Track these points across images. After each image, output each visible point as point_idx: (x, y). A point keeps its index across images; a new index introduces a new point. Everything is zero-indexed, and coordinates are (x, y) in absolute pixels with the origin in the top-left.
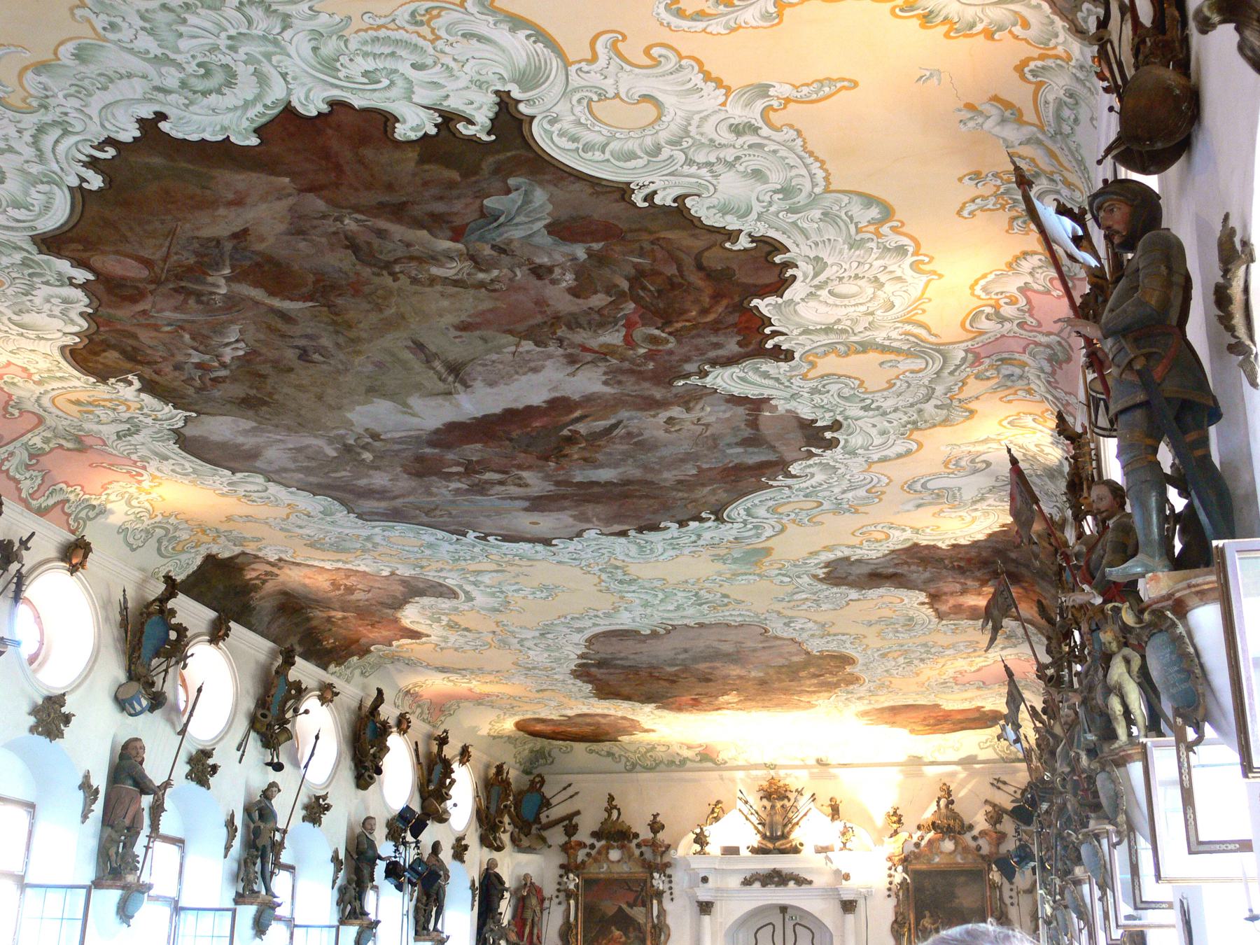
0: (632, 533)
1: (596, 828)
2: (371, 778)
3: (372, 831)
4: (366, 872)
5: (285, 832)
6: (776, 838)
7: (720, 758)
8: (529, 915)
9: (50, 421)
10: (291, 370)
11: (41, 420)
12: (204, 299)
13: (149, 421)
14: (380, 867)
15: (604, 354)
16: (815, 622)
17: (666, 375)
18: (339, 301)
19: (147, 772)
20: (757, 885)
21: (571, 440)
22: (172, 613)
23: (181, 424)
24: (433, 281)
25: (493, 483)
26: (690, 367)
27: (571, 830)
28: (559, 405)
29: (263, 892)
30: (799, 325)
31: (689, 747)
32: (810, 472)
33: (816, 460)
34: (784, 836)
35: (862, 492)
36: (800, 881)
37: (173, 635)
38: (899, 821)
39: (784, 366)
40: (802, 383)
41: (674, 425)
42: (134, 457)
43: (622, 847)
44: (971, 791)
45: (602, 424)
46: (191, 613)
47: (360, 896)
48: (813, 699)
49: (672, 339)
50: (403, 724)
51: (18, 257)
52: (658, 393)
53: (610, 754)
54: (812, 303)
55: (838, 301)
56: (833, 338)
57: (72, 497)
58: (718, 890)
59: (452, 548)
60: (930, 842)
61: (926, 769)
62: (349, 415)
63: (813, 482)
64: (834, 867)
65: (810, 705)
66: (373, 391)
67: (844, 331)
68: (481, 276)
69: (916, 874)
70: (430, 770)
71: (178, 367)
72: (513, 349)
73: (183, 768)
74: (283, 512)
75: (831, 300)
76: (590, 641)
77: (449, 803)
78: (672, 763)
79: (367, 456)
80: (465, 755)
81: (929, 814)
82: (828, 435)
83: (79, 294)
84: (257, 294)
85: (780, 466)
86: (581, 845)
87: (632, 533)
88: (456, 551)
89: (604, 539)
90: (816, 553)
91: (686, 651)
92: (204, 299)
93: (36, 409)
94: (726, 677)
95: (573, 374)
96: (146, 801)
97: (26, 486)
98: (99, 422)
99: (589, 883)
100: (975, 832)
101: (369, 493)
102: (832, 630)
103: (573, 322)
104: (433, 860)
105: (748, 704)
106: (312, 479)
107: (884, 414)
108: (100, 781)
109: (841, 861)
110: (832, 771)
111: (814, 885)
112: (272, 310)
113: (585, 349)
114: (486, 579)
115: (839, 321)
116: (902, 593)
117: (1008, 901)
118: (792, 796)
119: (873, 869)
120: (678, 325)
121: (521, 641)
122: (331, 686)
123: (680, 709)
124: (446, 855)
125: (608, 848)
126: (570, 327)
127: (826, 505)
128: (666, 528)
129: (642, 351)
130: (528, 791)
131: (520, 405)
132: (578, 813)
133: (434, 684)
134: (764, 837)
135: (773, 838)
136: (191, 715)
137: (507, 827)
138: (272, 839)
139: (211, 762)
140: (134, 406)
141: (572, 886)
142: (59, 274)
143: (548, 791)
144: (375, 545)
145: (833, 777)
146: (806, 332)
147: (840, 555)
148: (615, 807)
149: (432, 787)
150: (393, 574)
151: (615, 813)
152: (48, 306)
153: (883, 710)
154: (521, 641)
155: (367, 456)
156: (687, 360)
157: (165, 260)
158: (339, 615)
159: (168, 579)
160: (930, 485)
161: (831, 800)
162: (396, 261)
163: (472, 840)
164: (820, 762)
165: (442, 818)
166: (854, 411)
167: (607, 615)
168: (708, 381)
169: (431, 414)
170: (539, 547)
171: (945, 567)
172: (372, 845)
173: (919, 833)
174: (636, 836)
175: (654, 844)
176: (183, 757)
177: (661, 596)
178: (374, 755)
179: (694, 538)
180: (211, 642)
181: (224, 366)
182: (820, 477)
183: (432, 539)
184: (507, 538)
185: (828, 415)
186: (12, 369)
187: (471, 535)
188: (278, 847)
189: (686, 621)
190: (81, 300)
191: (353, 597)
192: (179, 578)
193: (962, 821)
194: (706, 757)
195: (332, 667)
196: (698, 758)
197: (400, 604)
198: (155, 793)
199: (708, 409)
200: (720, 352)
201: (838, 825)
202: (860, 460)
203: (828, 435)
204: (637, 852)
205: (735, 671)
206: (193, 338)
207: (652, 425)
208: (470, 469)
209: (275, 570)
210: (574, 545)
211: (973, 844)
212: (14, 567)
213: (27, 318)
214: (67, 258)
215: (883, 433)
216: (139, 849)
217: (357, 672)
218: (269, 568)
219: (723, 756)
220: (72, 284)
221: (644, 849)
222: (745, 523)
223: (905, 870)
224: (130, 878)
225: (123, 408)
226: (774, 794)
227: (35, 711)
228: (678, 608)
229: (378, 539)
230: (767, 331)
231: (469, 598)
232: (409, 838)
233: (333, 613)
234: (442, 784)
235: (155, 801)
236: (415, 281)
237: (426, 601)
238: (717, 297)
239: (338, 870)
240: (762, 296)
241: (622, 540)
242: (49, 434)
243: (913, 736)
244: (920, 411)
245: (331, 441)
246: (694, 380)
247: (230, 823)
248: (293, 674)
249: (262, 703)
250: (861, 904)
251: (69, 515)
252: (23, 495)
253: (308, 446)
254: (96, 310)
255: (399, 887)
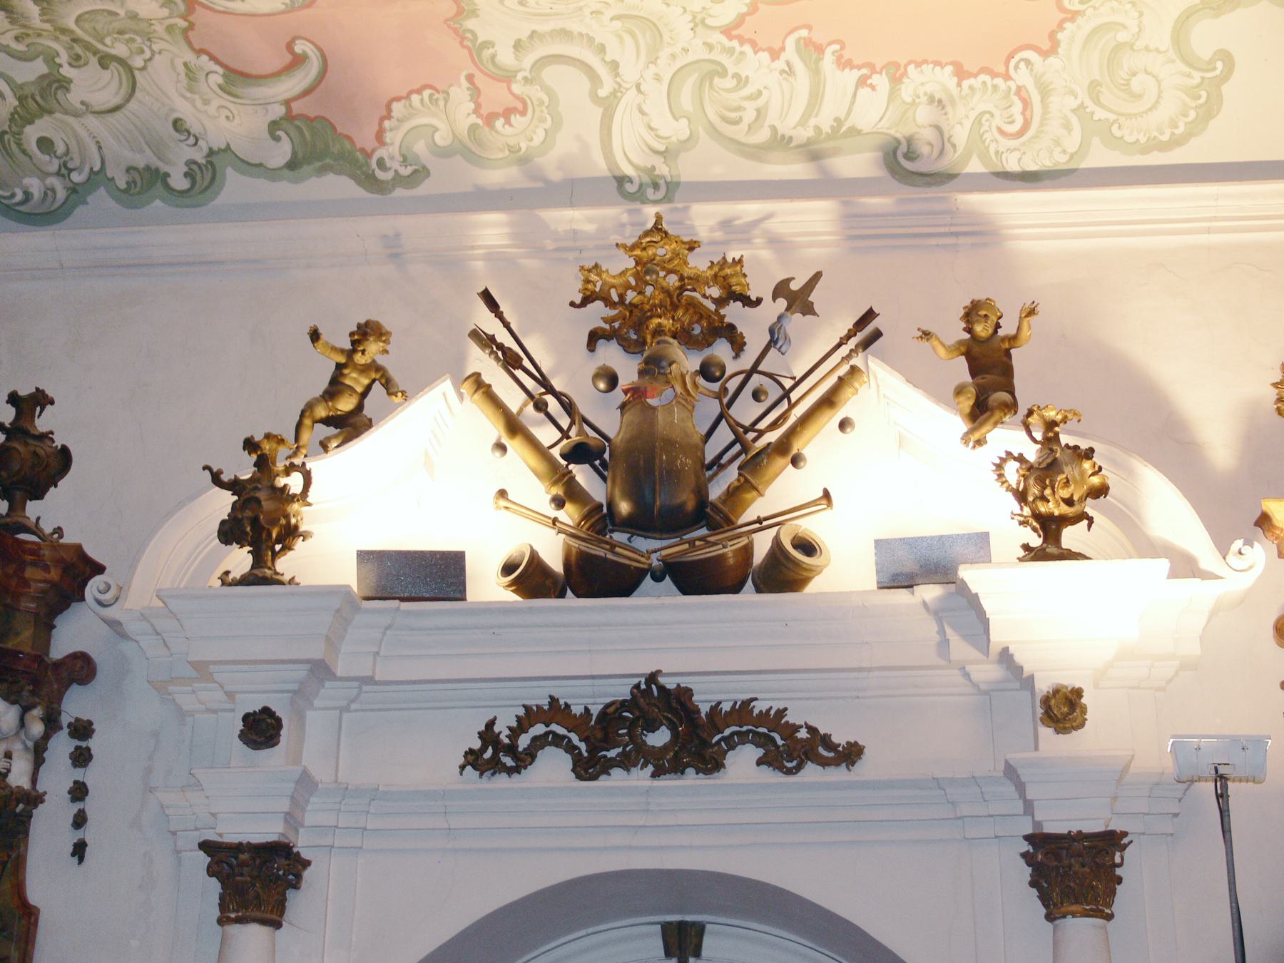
6: (663, 506)
7: (390, 151)
20: (553, 767)
34: (716, 517)
36: (794, 749)
78: (146, 182)
118: (753, 325)
161: (972, 313)
176: (1038, 703)
196: (282, 152)
201: (1009, 438)
226: (669, 312)
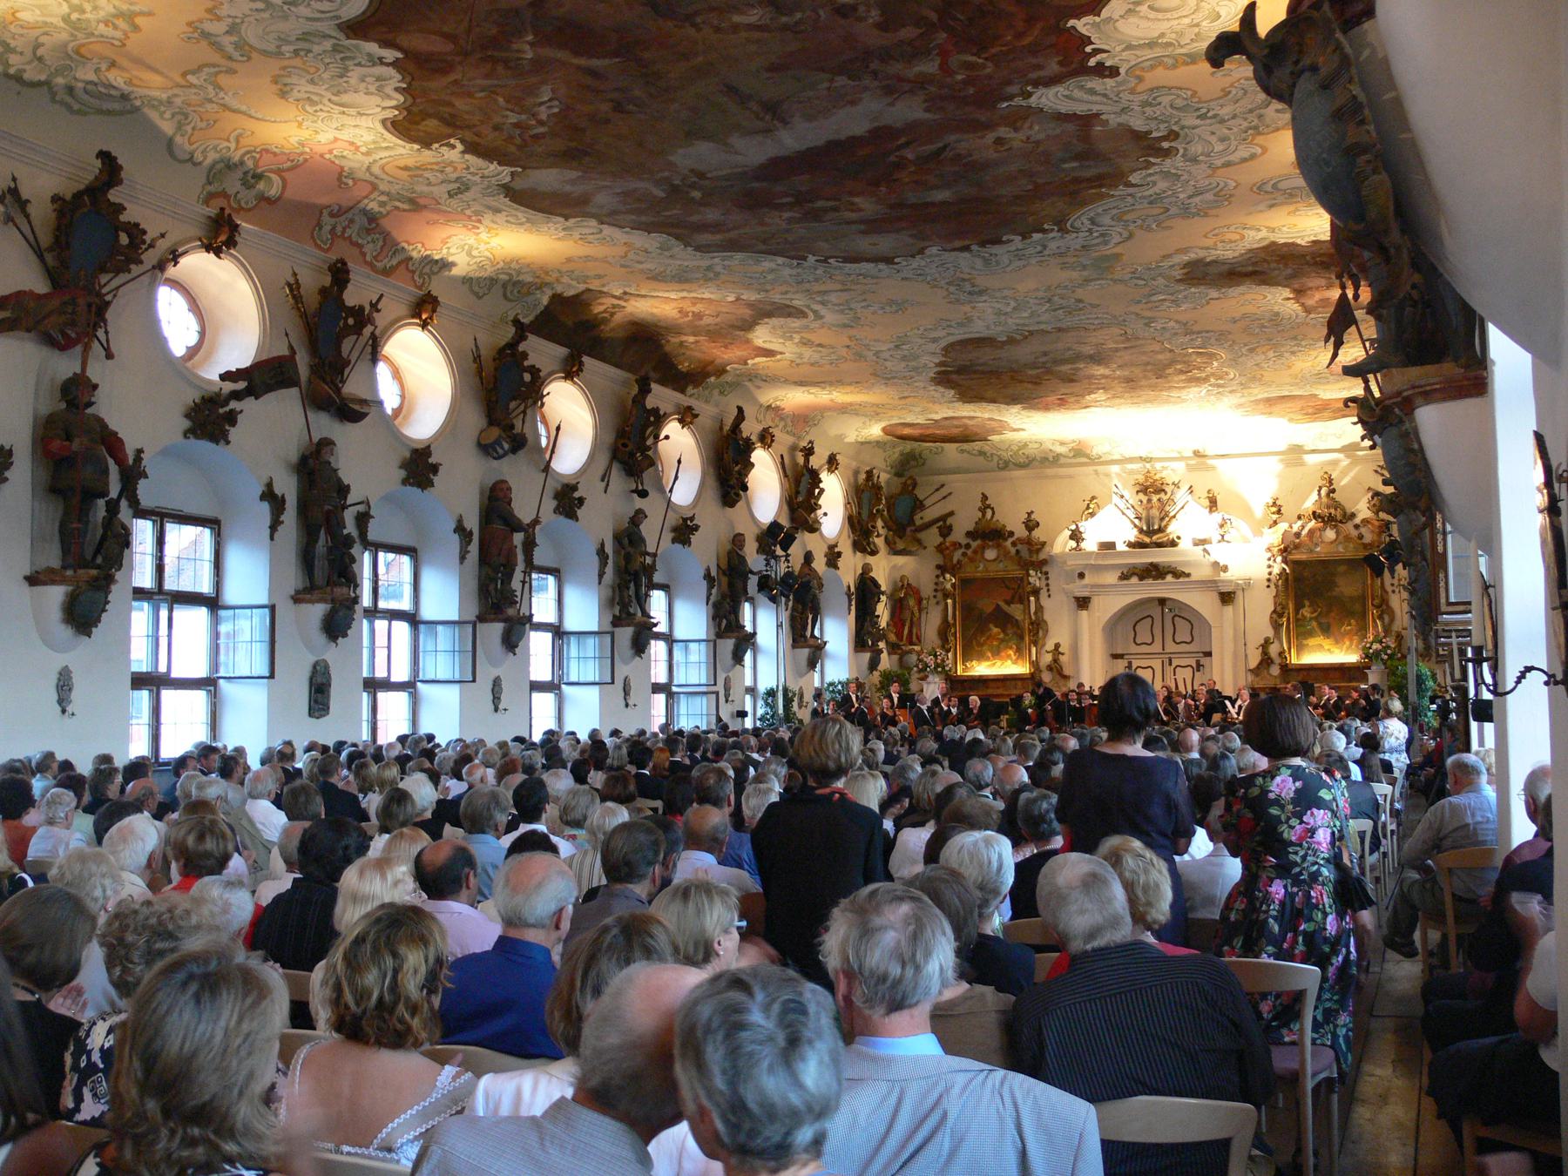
0: (974, 247)
1: (971, 527)
2: (738, 495)
3: (742, 547)
4: (739, 585)
5: (655, 555)
8: (907, 615)
9: (382, 187)
10: (608, 121)
11: (374, 187)
12: (512, 64)
13: (477, 178)
14: (753, 582)
15: (921, 82)
16: (1177, 322)
17: (988, 97)
18: (646, 55)
19: (516, 512)
20: (1134, 580)
21: (900, 165)
22: (525, 355)
23: (508, 179)
24: (736, 28)
25: (825, 210)
26: (1014, 89)
27: (946, 531)
28: (881, 135)
29: (639, 614)
30: (1120, 42)
31: (1062, 444)
32: (1151, 180)
33: (1157, 169)
35: (1209, 196)
36: (1178, 574)
37: (527, 377)
38: (1279, 512)
39: (1110, 82)
40: (1131, 97)
41: (1002, 145)
42: (468, 212)
43: (998, 546)
44: (1354, 478)
45: (930, 148)
46: (541, 352)
47: (735, 611)
48: (1183, 394)
49: (989, 64)
50: (766, 438)
51: (328, 45)
52: (983, 117)
53: (982, 453)
54: (1132, 20)
55: (1160, 16)
56: (1158, 52)
57: (414, 254)
58: (1093, 586)
59: (794, 272)
60: (1311, 532)
61: (1311, 459)
62: (671, 158)
63: (1156, 189)
64: (1212, 559)
65: (1181, 400)
66: (694, 134)
67: (1169, 44)
68: (784, 19)
69: (1296, 565)
70: (797, 482)
71: (496, 128)
72: (826, 85)
73: (550, 504)
74: (621, 250)
75: (1153, 15)
76: (947, 350)
77: (820, 512)
78: (1045, 459)
79: (696, 194)
80: (832, 463)
81: (1310, 503)
82: (1165, 145)
83: (391, 71)
84: (560, 55)
85: (1117, 178)
86: (957, 545)
87: (974, 247)
88: (798, 275)
89: (947, 254)
90: (1169, 256)
91: (1045, 354)
92: (512, 64)
93: (367, 177)
94: (1090, 377)
95: (892, 104)
96: (518, 538)
97: (370, 250)
98: (429, 184)
99: (965, 583)
100: (1357, 520)
101: (704, 227)
102: (1195, 328)
103: (886, 56)
104: (806, 570)
105: (1117, 401)
106: (643, 219)
107: (1222, 121)
108: (472, 523)
109: (1218, 553)
110: (1210, 462)
111: (1193, 578)
112: (579, 67)
113: (900, 79)
114: (833, 298)
115: (1162, 35)
116: (1265, 290)
117: (1389, 589)
118: (1169, 489)
119: (1251, 558)
120: (994, 51)
121: (877, 354)
122: (690, 408)
123: (1047, 408)
124: (819, 564)
125: (983, 548)
126: (882, 60)
127: (1173, 210)
128: (1009, 241)
129: (959, 77)
130: (901, 494)
131: (843, 136)
132: (951, 514)
133: (794, 398)
134: (1141, 531)
135: (1150, 533)
136: (553, 452)
137: (881, 531)
138: (643, 564)
139: (576, 495)
140: (460, 167)
141: (948, 586)
142: (369, 55)
143: (920, 493)
144: (717, 274)
145: (1213, 468)
146: (1129, 47)
147: (1193, 256)
148: (989, 506)
149: (800, 499)
150: (738, 299)
151: (989, 512)
152: (363, 85)
153: (1257, 402)
154: (877, 354)
155: (696, 194)
156: (1010, 83)
157: (469, 31)
158: (691, 339)
159: (516, 322)
160: (1281, 186)
162: (696, 13)
163: (845, 547)
164: (1197, 454)
165: (814, 528)
166: (1189, 120)
167: (961, 325)
168: (1033, 101)
169: (753, 151)
170: (882, 266)
171: (1307, 263)
172: (743, 560)
173: (1300, 523)
174: (1011, 534)
175: (1028, 542)
176: (549, 493)
177: (1013, 304)
178: (739, 473)
179: (1039, 248)
180: (566, 378)
181: (541, 123)
182: (1162, 185)
183: (773, 265)
184: (847, 260)
185: (1162, 126)
186: (339, 144)
187: (811, 259)
188: (651, 569)
189: (1043, 327)
190: (394, 78)
191: (702, 323)
192: (526, 321)
193: (1343, 510)
194: (1080, 454)
195: (690, 390)
197: (749, 326)
198: (525, 531)
199: (1036, 128)
200: (1041, 73)
201: (1217, 517)
202: (1203, 166)
203: (1165, 145)
204: (1013, 551)
205: (1101, 371)
206: (508, 102)
207: (980, 146)
208: (800, 199)
209: (622, 303)
210: (917, 262)
211: (1354, 533)
212: (368, 330)
213: (345, 98)
214: (375, 40)
215: (1222, 140)
216: (516, 584)
217: (716, 392)
218: (616, 302)
219: (1098, 450)
220: (382, 63)
221: (1019, 547)
222: (1090, 231)
223: (1285, 561)
224: (511, 612)
225: (449, 169)
226: (1151, 488)
227: (405, 465)
228: (1032, 315)
229: (718, 269)
230: (1088, 49)
231: (818, 316)
232: (779, 552)
233: (684, 338)
234: (810, 493)
235: (526, 538)
236: (718, 30)
237: (774, 321)
238: (1030, 20)
239: (710, 587)
240: (1078, 17)
241: (966, 254)
242: (384, 198)
243: (1293, 425)
244: (1260, 116)
245: (657, 183)
246: (1018, 101)
247: (601, 552)
248: (650, 402)
249: (621, 434)
250: (1240, 593)
251: (413, 272)
252: (368, 258)
253: (635, 190)
254: (410, 84)
255: (773, 599)
